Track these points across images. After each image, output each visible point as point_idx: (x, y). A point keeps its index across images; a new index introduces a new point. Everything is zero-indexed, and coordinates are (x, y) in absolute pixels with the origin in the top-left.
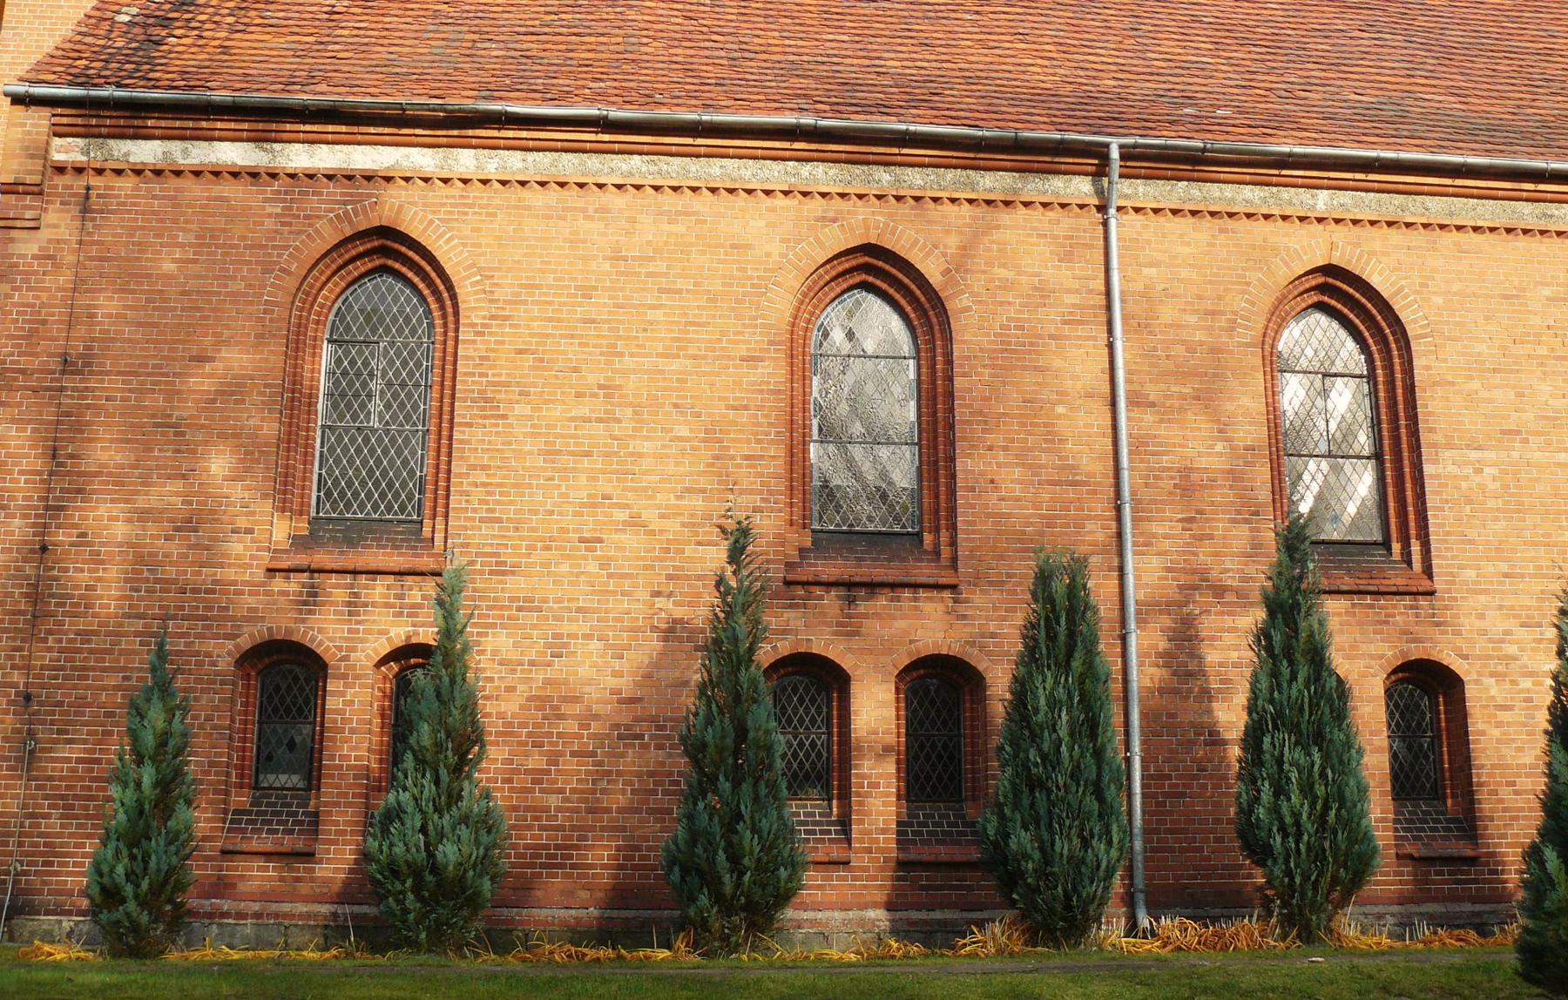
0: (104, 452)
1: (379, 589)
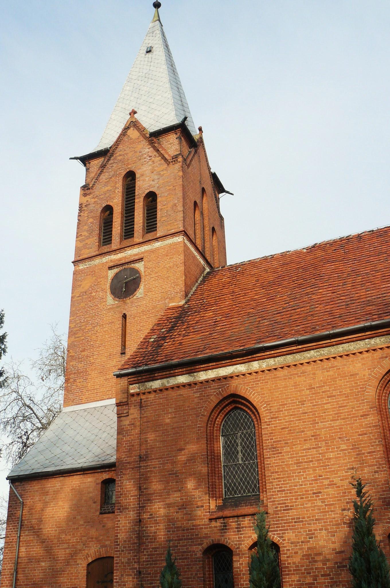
0: (156, 486)
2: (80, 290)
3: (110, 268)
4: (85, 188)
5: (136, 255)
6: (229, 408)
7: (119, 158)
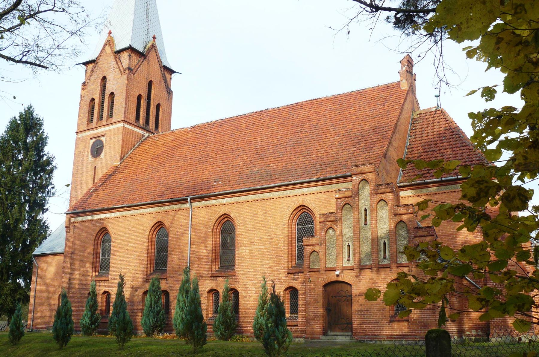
0: (77, 265)
1: (102, 283)
3: (91, 139)
7: (100, 66)
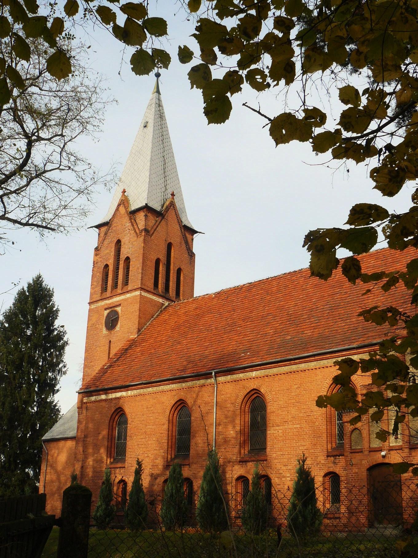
0: (90, 450)
2: (91, 322)
3: (106, 309)
4: (97, 249)
5: (117, 301)
6: (180, 407)
